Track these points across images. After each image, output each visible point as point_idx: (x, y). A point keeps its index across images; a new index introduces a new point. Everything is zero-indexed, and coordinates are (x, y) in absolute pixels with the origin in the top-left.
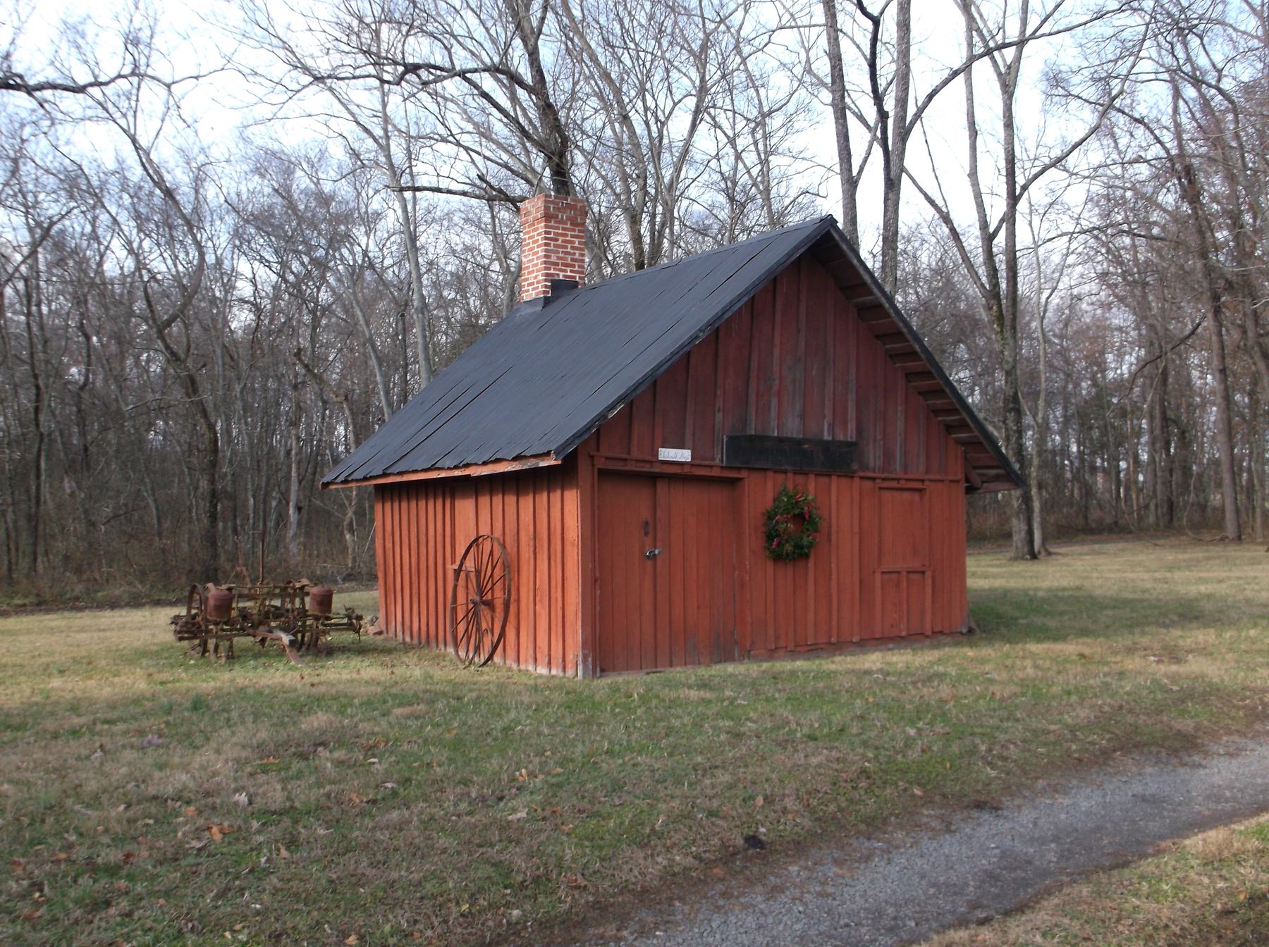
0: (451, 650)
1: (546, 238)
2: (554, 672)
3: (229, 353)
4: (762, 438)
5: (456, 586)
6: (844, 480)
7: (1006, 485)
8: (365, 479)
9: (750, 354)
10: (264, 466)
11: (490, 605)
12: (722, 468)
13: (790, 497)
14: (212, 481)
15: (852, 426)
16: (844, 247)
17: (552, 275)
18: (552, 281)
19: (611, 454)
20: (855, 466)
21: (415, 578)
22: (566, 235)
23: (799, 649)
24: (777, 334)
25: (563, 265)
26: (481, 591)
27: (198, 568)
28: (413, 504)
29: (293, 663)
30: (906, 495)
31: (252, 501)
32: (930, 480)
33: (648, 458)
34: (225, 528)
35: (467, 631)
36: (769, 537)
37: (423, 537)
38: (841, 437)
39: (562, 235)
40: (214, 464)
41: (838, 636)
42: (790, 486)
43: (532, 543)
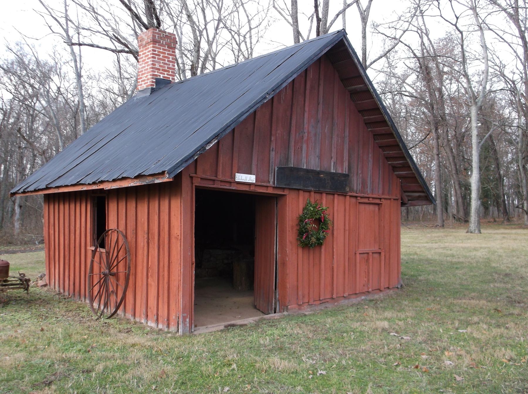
2: (160, 326)
4: (298, 170)
5: (92, 262)
6: (341, 198)
8: (35, 191)
11: (116, 275)
15: (346, 164)
17: (156, 75)
18: (156, 79)
19: (204, 176)
20: (348, 189)
21: (67, 253)
22: (165, 53)
23: (315, 303)
25: (163, 70)
26: (109, 266)
30: (371, 207)
33: (229, 180)
34: (460, 166)
35: (99, 291)
36: (301, 233)
38: (340, 171)
42: (312, 200)
43: (146, 236)
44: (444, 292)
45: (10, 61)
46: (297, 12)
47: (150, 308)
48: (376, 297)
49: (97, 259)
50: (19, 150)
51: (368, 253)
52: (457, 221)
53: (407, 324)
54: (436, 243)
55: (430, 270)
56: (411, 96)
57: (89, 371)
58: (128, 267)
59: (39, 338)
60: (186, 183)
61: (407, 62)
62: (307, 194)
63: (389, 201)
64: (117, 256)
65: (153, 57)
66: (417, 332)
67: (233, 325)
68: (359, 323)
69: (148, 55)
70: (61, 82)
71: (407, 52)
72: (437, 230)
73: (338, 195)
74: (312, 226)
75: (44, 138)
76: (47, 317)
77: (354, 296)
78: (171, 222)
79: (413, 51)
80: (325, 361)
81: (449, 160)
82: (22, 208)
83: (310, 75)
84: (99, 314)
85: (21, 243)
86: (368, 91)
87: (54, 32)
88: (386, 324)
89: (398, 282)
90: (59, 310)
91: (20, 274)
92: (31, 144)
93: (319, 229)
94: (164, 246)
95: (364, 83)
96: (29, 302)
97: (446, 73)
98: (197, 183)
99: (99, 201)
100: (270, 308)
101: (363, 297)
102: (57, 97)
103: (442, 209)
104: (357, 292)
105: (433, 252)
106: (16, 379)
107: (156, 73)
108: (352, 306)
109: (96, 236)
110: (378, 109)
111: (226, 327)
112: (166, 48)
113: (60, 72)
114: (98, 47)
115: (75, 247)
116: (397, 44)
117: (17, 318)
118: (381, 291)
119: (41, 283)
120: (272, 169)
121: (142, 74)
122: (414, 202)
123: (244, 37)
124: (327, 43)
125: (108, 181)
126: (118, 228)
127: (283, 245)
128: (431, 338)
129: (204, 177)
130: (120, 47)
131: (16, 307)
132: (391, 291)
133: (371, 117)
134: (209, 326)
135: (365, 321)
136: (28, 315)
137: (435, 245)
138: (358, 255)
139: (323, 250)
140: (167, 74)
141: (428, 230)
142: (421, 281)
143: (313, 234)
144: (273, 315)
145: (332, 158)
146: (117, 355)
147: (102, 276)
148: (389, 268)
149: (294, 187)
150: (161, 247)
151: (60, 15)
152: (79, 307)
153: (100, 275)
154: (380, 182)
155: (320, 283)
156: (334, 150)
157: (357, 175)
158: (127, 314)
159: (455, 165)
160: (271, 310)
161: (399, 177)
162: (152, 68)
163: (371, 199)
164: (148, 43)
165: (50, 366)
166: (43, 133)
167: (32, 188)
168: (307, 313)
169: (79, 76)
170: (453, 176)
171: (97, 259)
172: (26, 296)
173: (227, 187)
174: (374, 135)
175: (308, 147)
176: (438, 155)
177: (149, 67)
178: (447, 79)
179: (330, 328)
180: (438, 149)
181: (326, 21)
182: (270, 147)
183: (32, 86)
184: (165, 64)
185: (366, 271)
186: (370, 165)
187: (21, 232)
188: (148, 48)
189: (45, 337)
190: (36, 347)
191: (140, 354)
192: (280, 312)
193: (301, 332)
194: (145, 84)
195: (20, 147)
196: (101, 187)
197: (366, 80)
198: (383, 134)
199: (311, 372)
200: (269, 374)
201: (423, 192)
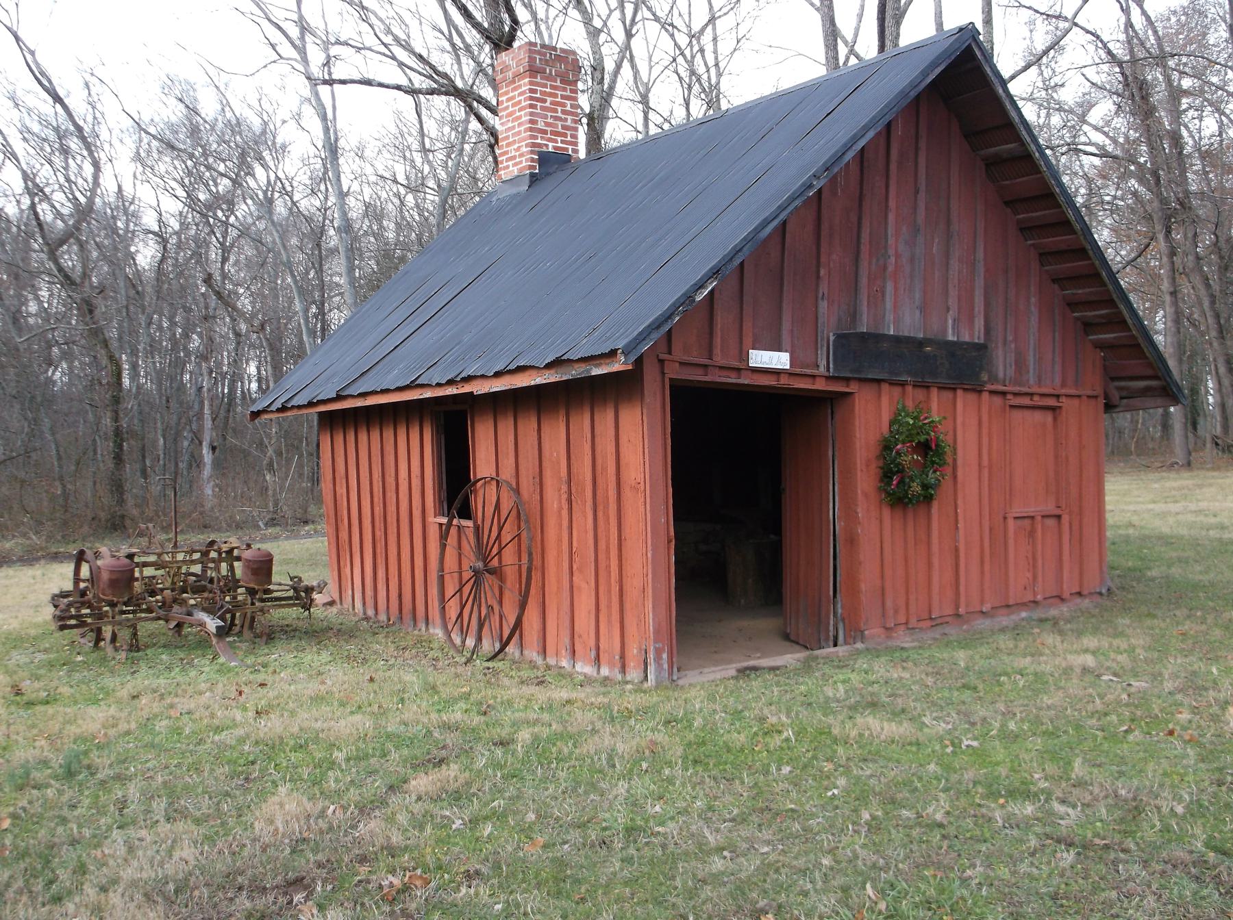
0: (438, 632)
2: (605, 671)
3: (134, 283)
6: (971, 397)
7: (1159, 401)
8: (311, 404)
10: (173, 404)
11: (497, 572)
12: (827, 378)
14: (116, 419)
15: (979, 323)
17: (539, 145)
18: (540, 154)
19: (686, 358)
20: (985, 377)
21: (379, 533)
22: (555, 96)
23: (921, 624)
25: (553, 133)
26: (483, 553)
27: (102, 515)
29: (222, 660)
30: (1038, 416)
31: (161, 441)
32: (1066, 396)
33: (736, 364)
37: (390, 480)
38: (967, 338)
39: (551, 95)
40: (116, 400)
41: (967, 606)
42: (910, 404)
43: (564, 488)
44: (1212, 600)
47: (580, 636)
48: (1053, 612)
51: (1032, 518)
52: (1223, 451)
53: (1134, 660)
54: (1176, 502)
55: (1171, 558)
56: (1103, 154)
61: (1091, 73)
62: (897, 391)
63: (1076, 402)
65: (531, 106)
66: (1160, 674)
67: (755, 669)
68: (1029, 659)
69: (520, 102)
71: (1091, 48)
72: (1173, 475)
74: (909, 459)
77: (1005, 611)
78: (622, 455)
79: (1105, 45)
81: (1200, 304)
82: (217, 451)
83: (898, 132)
85: (229, 526)
86: (1028, 157)
88: (1090, 660)
89: (1102, 580)
90: (381, 645)
91: (292, 579)
93: (924, 466)
94: (606, 507)
96: (316, 634)
97: (1186, 93)
98: (675, 372)
99: (451, 421)
100: (822, 638)
101: (1024, 614)
103: (1185, 424)
105: (1171, 520)
107: (539, 141)
108: (1003, 630)
109: (444, 494)
111: (739, 671)
112: (558, 84)
113: (274, 143)
114: (381, 85)
116: (1068, 31)
118: (1062, 600)
122: (1135, 402)
124: (938, 58)
125: (483, 376)
126: (498, 475)
128: (1194, 685)
132: (1087, 601)
133: (1034, 214)
134: (706, 670)
135: (1041, 654)
136: (325, 656)
137: (1173, 507)
138: (1011, 522)
140: (562, 142)
141: (1152, 476)
142: (1153, 579)
143: (914, 471)
144: (832, 649)
145: (948, 310)
148: (1081, 550)
149: (870, 376)
154: (1057, 359)
156: (953, 293)
157: (1005, 343)
158: (526, 652)
159: (1217, 316)
160: (827, 639)
161: (1099, 346)
162: (531, 129)
163: (1036, 398)
164: (518, 76)
167: (301, 400)
170: (1211, 344)
173: (733, 380)
174: (1040, 254)
175: (896, 289)
176: (1174, 294)
177: (522, 128)
178: (1191, 107)
179: (967, 668)
180: (1174, 279)
182: (817, 291)
184: (556, 118)
185: (1030, 556)
186: (1034, 320)
188: (520, 86)
192: (846, 643)
193: (908, 676)
194: (514, 165)
196: (466, 389)
197: (1024, 133)
198: (1065, 252)
201: (1156, 377)
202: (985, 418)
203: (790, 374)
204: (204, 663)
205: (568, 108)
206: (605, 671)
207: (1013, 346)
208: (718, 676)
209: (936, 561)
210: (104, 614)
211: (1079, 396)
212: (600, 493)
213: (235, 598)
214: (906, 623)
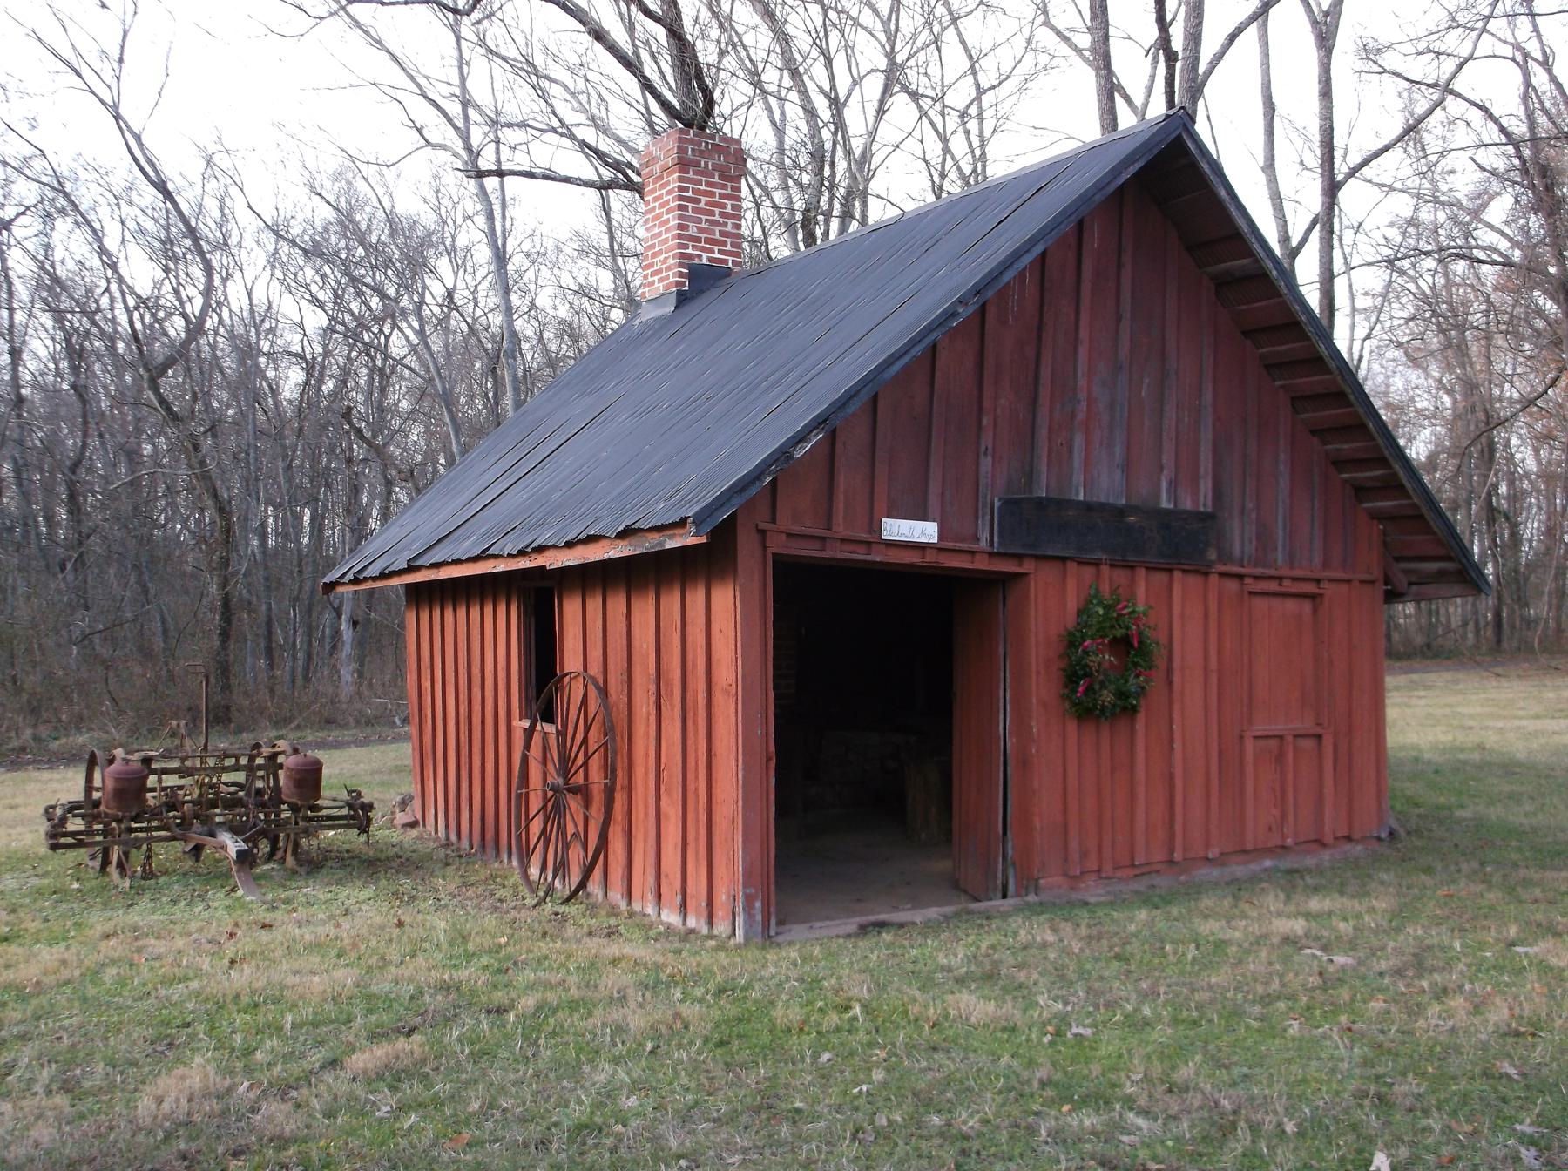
1: (681, 198)
2: (692, 922)
4: (1062, 504)
6: (1194, 581)
8: (383, 576)
9: (1038, 354)
11: (584, 792)
12: (991, 554)
13: (1107, 608)
14: (224, 584)
15: (1206, 486)
16: (1205, 167)
17: (690, 256)
18: (690, 267)
19: (796, 528)
22: (712, 194)
23: (1119, 874)
24: (1084, 318)
25: (707, 241)
26: (565, 768)
28: (475, 612)
29: (240, 893)
30: (1291, 605)
32: (1331, 580)
33: (864, 536)
37: (476, 671)
38: (1187, 504)
39: (706, 193)
41: (1185, 850)
42: (1105, 588)
43: (653, 688)
45: (319, 225)
46: (1106, 37)
49: (535, 751)
50: (349, 468)
51: (1281, 737)
57: (500, 1011)
58: (610, 770)
59: (391, 940)
60: (746, 545)
61: (1483, 157)
63: (1344, 588)
64: (585, 740)
70: (456, 274)
73: (1184, 571)
75: (416, 433)
76: (413, 898)
80: (1097, 1007)
83: (1093, 241)
84: (541, 894)
85: (358, 722)
87: (428, 143)
91: (349, 793)
92: (380, 452)
95: (1250, 253)
96: (372, 866)
98: (778, 545)
99: (537, 595)
101: (1268, 863)
102: (448, 317)
104: (1249, 847)
106: (332, 1022)
107: (690, 251)
109: (532, 692)
110: (1296, 324)
115: (483, 722)
117: (342, 897)
118: (1324, 845)
119: (401, 818)
120: (984, 506)
121: (654, 255)
122: (1429, 589)
123: (963, 115)
124: (1133, 152)
125: (554, 546)
127: (1021, 713)
129: (796, 529)
130: (607, 174)
131: (341, 873)
132: (1359, 848)
133: (1284, 347)
134: (818, 924)
136: (368, 892)
139: (1140, 726)
140: (720, 252)
142: (1459, 821)
143: (1109, 680)
144: (998, 902)
145: (1161, 469)
146: (573, 979)
147: (550, 794)
149: (1050, 553)
150: (690, 715)
151: (446, 90)
152: (493, 877)
153: (545, 793)
155: (1132, 821)
160: (995, 889)
161: (1377, 516)
165: (412, 998)
166: (410, 416)
167: (373, 571)
168: (1092, 900)
169: (501, 258)
171: (535, 751)
172: (365, 848)
173: (859, 555)
174: (1293, 399)
175: (1088, 442)
181: (1197, 59)
182: (978, 443)
183: (378, 290)
186: (1284, 483)
187: (359, 694)
188: (668, 183)
189: (405, 938)
190: (382, 958)
191: (628, 979)
192: (1018, 894)
194: (661, 280)
195: (349, 461)
199: (1050, 1029)
200: (940, 1032)
201: (1450, 559)
202: (1213, 607)
203: (940, 549)
204: (218, 898)
205: (729, 210)
206: (692, 922)
207: (1254, 515)
208: (835, 932)
209: (1141, 790)
210: (119, 830)
211: (1349, 581)
212: (690, 694)
213: (278, 815)
214: (1099, 871)
